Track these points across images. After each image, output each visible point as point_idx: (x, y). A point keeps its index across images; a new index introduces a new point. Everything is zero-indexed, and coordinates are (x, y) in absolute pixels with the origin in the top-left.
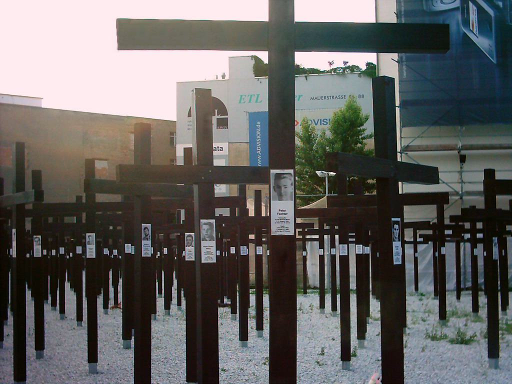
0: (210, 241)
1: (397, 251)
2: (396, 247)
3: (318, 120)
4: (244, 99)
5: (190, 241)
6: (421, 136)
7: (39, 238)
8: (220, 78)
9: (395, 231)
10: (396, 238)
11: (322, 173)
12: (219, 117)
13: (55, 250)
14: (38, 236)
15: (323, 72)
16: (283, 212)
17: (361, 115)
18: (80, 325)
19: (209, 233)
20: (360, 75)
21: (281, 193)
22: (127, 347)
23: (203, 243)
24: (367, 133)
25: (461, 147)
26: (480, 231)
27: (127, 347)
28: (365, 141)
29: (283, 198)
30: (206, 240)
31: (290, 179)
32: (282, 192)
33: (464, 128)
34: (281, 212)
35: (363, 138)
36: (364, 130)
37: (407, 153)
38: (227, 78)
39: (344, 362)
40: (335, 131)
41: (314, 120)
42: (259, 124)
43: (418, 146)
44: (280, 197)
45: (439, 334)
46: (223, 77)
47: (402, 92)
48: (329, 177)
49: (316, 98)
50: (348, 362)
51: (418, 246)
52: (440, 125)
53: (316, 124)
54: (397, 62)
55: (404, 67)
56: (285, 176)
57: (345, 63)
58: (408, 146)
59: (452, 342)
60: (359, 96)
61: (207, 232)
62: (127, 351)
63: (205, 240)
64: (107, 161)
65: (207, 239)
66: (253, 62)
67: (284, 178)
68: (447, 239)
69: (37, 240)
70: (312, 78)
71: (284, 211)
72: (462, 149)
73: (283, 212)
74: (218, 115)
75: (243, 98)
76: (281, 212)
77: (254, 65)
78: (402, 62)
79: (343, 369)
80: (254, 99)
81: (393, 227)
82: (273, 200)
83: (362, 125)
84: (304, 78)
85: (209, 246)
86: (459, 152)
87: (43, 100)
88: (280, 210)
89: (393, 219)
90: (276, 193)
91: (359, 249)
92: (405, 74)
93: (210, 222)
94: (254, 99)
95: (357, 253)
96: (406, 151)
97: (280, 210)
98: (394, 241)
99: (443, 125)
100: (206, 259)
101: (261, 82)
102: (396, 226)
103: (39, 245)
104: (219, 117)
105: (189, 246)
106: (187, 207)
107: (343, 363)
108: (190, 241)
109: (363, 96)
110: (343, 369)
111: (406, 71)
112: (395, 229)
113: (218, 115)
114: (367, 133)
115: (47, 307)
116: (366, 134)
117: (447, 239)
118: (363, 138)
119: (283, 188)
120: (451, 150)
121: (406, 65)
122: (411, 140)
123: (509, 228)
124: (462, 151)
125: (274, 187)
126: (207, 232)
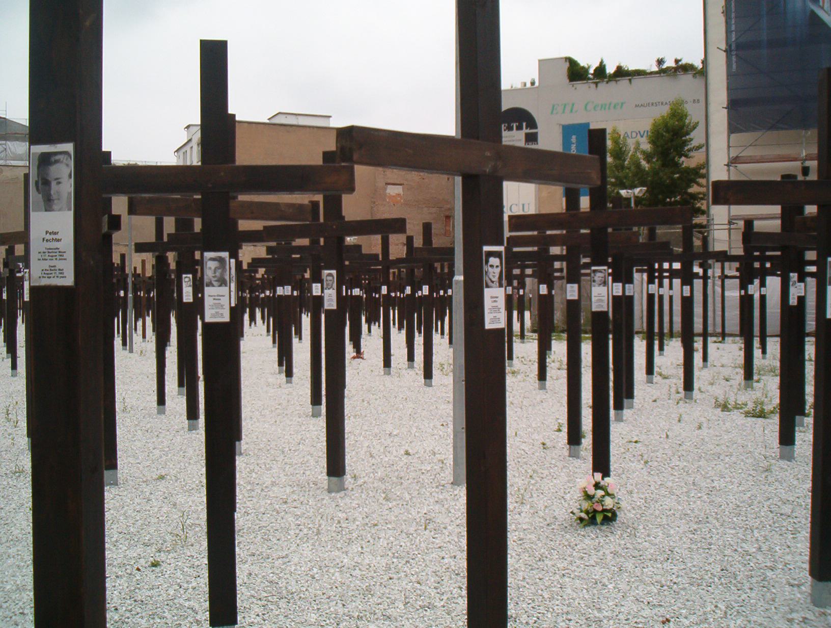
0: (220, 286)
1: (495, 304)
2: (492, 297)
3: (644, 132)
4: (556, 109)
5: (331, 282)
6: (753, 144)
7: (189, 277)
8: (529, 85)
9: (490, 269)
10: (493, 282)
11: (628, 192)
12: (528, 131)
13: (386, 287)
14: (188, 276)
15: (652, 73)
16: (55, 237)
17: (687, 121)
18: (411, 367)
19: (218, 274)
20: (694, 76)
21: (50, 195)
22: (315, 415)
23: (208, 291)
24: (694, 143)
25: (806, 156)
26: (365, 282)
27: (315, 415)
28: (691, 154)
29: (55, 207)
30: (213, 286)
31: (67, 165)
32: (52, 192)
33: (809, 133)
34: (48, 237)
35: (689, 150)
36: (691, 140)
37: (736, 166)
38: (537, 84)
39: (572, 447)
40: (653, 142)
41: (639, 132)
42: (574, 139)
43: (750, 156)
44: (48, 203)
45: (732, 401)
46: (533, 83)
47: (731, 89)
48: (636, 198)
49: (642, 105)
50: (577, 447)
51: (726, 280)
52: (777, 129)
53: (642, 137)
54: (724, 51)
55: (734, 59)
56: (57, 157)
57: (677, 61)
58: (737, 157)
59: (747, 414)
60: (694, 100)
61: (215, 273)
62: (314, 420)
63: (210, 284)
64: (401, 187)
65: (215, 283)
66: (567, 64)
67: (57, 162)
68: (349, 294)
69: (187, 280)
70: (637, 81)
71: (56, 233)
72: (806, 160)
73: (55, 237)
74: (526, 128)
75: (555, 107)
76: (48, 237)
77: (569, 68)
78: (731, 51)
79: (570, 456)
80: (568, 108)
81: (487, 262)
82: (33, 211)
83: (688, 134)
84: (628, 81)
85: (218, 296)
86: (802, 163)
87: (331, 119)
88: (47, 232)
89: (486, 248)
90: (40, 196)
91: (617, 289)
92: (734, 66)
93: (220, 257)
94: (568, 108)
95: (614, 294)
96: (735, 163)
97: (47, 232)
98: (488, 286)
99: (782, 129)
100: (213, 316)
101: (576, 89)
102: (494, 261)
103: (190, 286)
104: (528, 131)
105: (329, 289)
106: (326, 234)
107: (570, 448)
108: (331, 282)
109: (698, 100)
110: (570, 456)
111: (736, 62)
112: (492, 266)
113: (526, 128)
114: (694, 143)
115: (436, 337)
116: (692, 146)
117: (349, 294)
118: (689, 150)
119: (53, 184)
120: (791, 161)
121: (737, 55)
122: (740, 149)
123: (830, 259)
124: (807, 162)
125: (37, 183)
126: (215, 273)
